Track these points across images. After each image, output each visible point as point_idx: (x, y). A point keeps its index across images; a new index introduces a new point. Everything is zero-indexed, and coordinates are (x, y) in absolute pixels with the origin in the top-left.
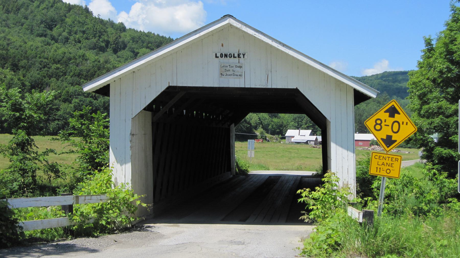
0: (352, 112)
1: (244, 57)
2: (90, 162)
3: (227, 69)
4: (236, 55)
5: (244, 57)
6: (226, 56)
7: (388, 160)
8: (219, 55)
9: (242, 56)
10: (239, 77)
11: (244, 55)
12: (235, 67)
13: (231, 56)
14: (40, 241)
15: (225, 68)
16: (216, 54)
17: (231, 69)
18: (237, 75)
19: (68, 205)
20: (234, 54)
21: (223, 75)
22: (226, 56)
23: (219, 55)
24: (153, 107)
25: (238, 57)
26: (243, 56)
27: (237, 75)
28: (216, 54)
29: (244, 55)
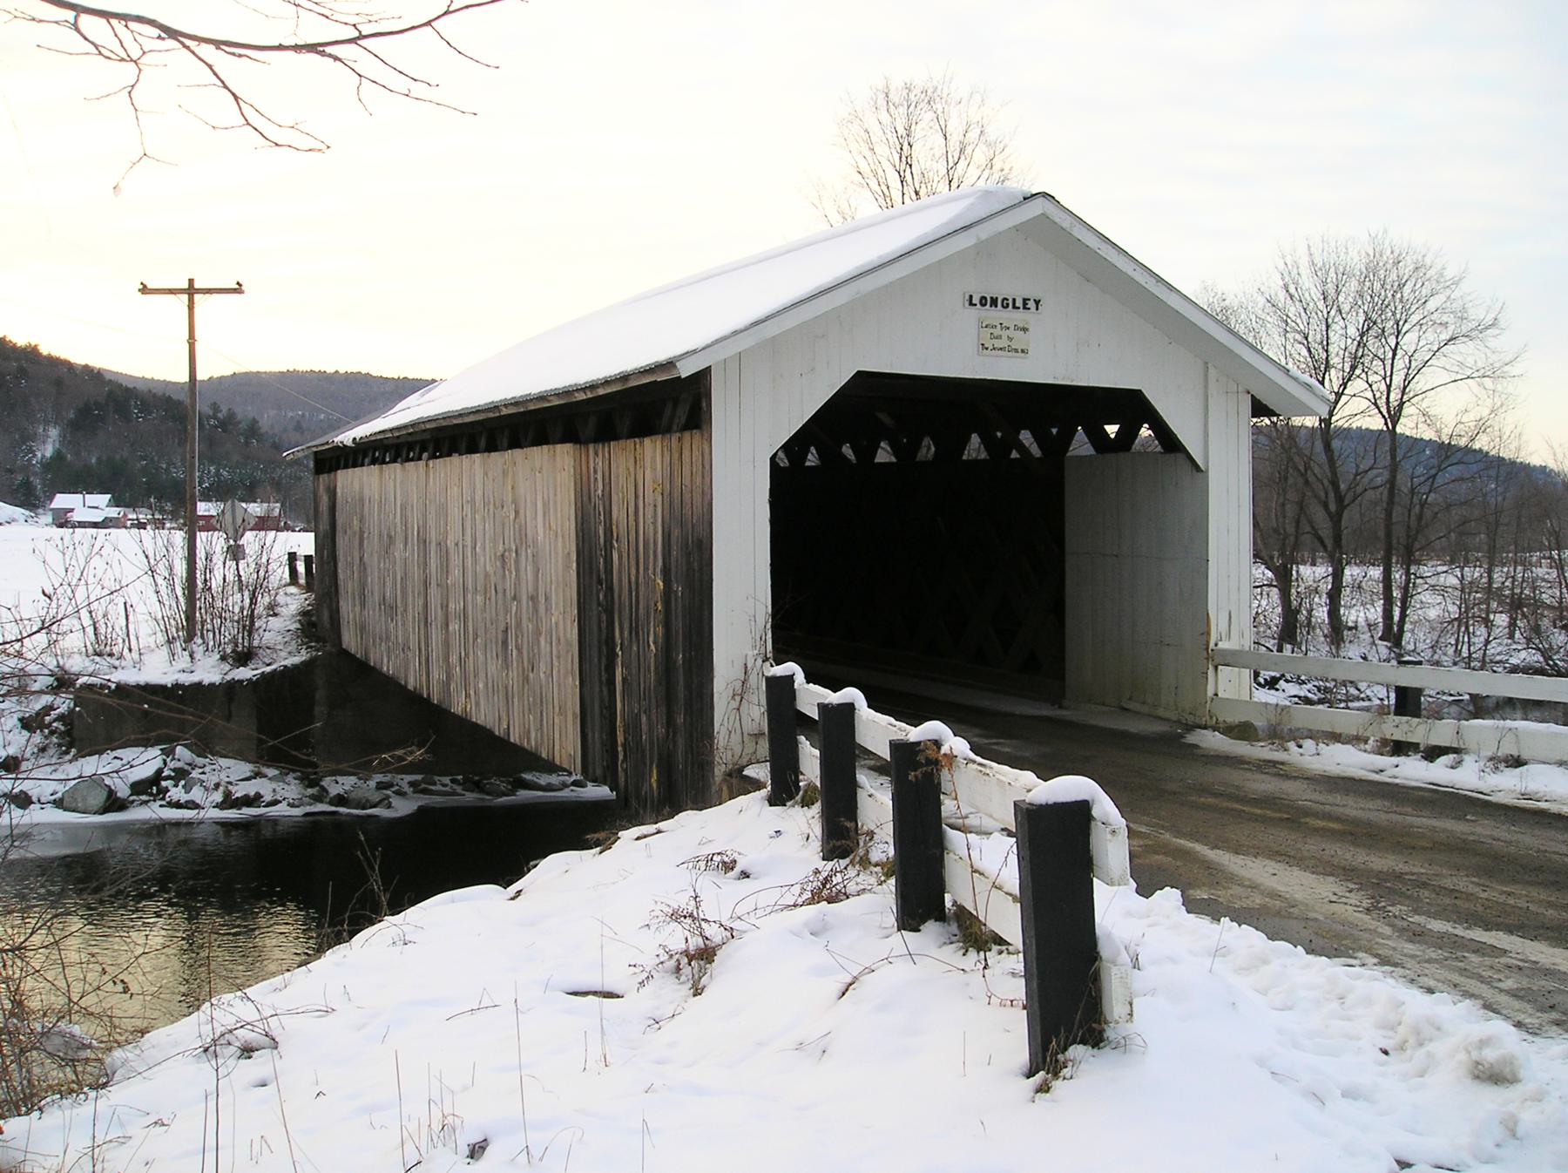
0: (1014, 360)
1: (1037, 309)
2: (70, 746)
3: (997, 332)
4: (1019, 303)
5: (1037, 309)
6: (994, 302)
7: (638, 839)
8: (976, 300)
9: (1031, 304)
10: (1020, 354)
11: (1037, 302)
12: (1012, 328)
13: (1008, 304)
14: (1423, 797)
15: (992, 330)
16: (971, 297)
17: (1005, 334)
18: (1016, 351)
19: (1504, 698)
20: (1014, 300)
21: (987, 349)
22: (994, 302)
23: (976, 300)
24: (844, 458)
25: (1025, 308)
26: (1034, 305)
27: (1016, 351)
28: (971, 297)
29: (1037, 302)
